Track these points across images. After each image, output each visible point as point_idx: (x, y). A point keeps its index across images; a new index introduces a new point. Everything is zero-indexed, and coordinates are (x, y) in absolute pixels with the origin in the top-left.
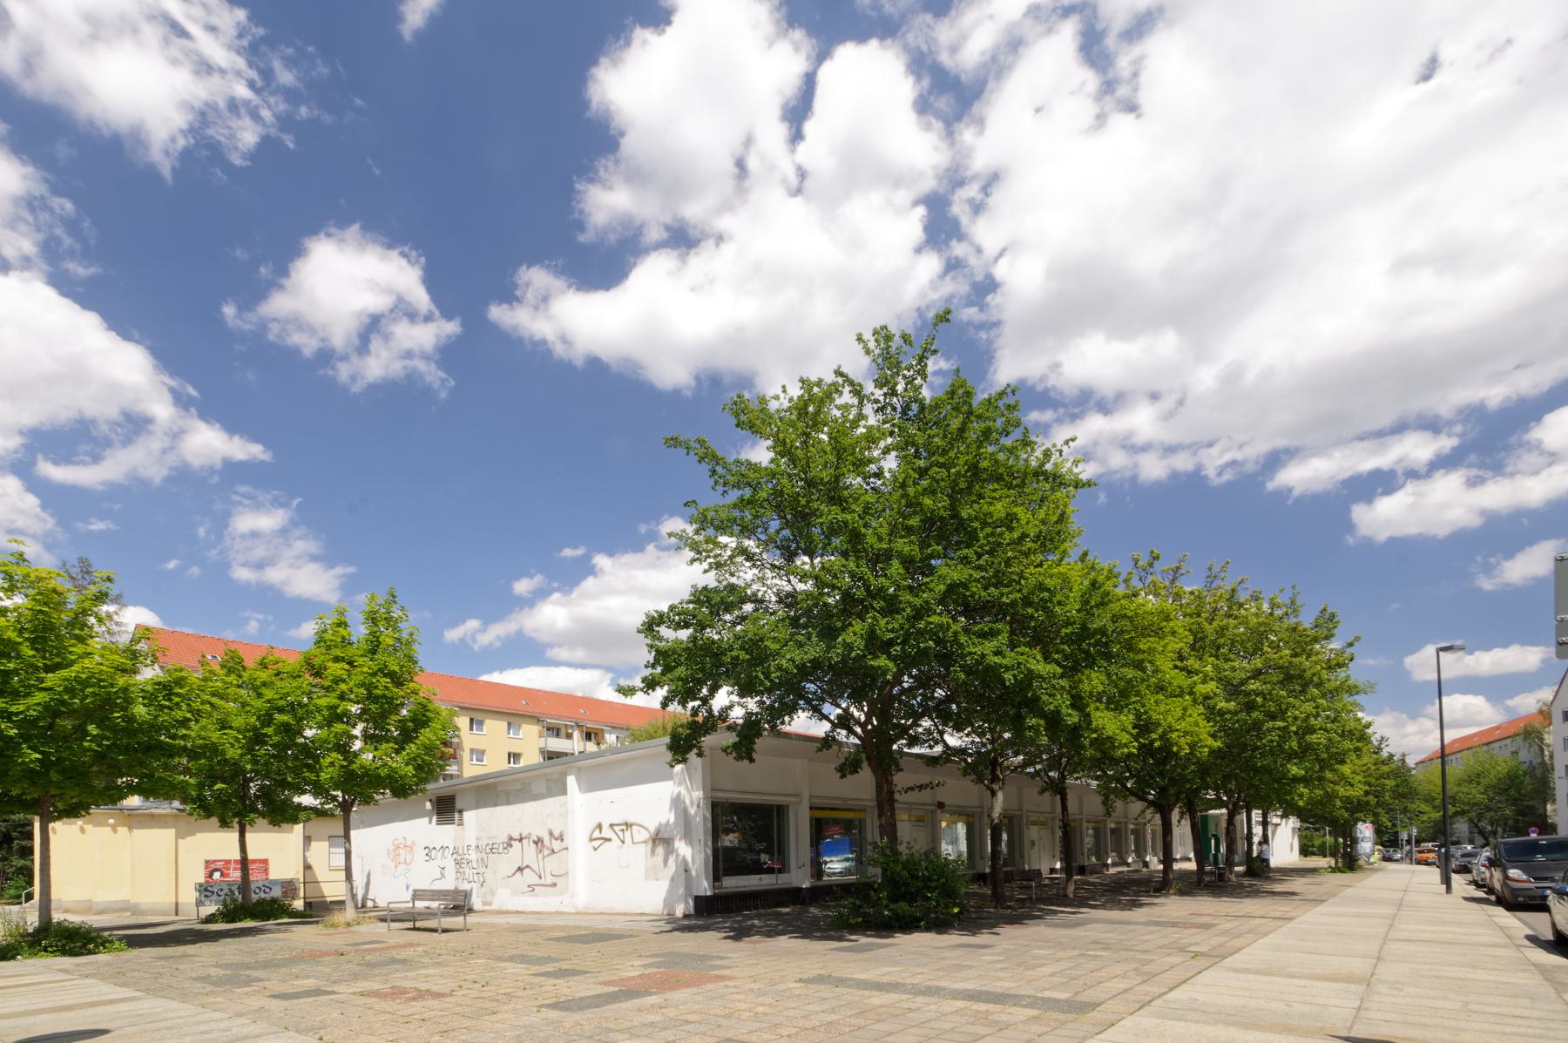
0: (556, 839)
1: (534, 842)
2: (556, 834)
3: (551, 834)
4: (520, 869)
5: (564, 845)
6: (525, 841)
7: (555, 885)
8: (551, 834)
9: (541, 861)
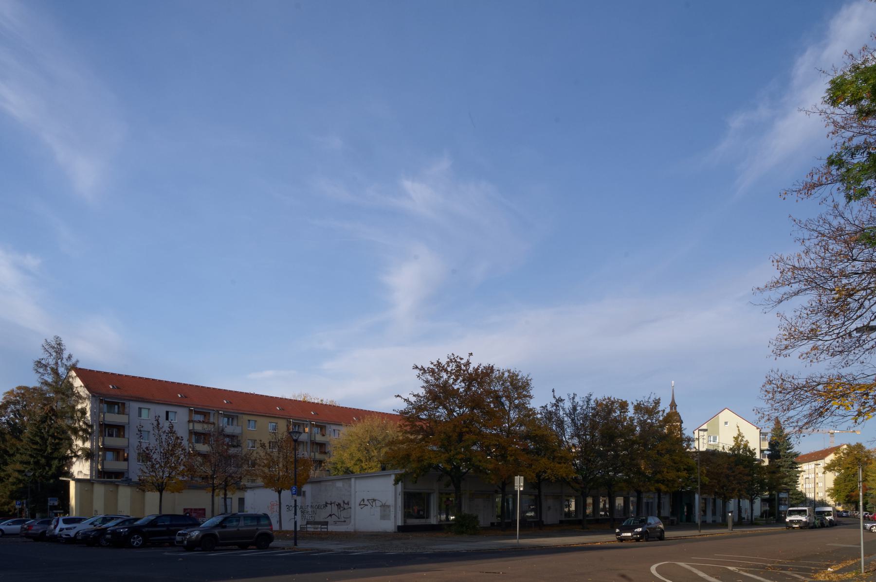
0: (346, 504)
1: (337, 505)
2: (346, 502)
3: (344, 502)
4: (330, 515)
5: (349, 506)
6: (333, 505)
7: (345, 521)
8: (344, 502)
9: (339, 512)
